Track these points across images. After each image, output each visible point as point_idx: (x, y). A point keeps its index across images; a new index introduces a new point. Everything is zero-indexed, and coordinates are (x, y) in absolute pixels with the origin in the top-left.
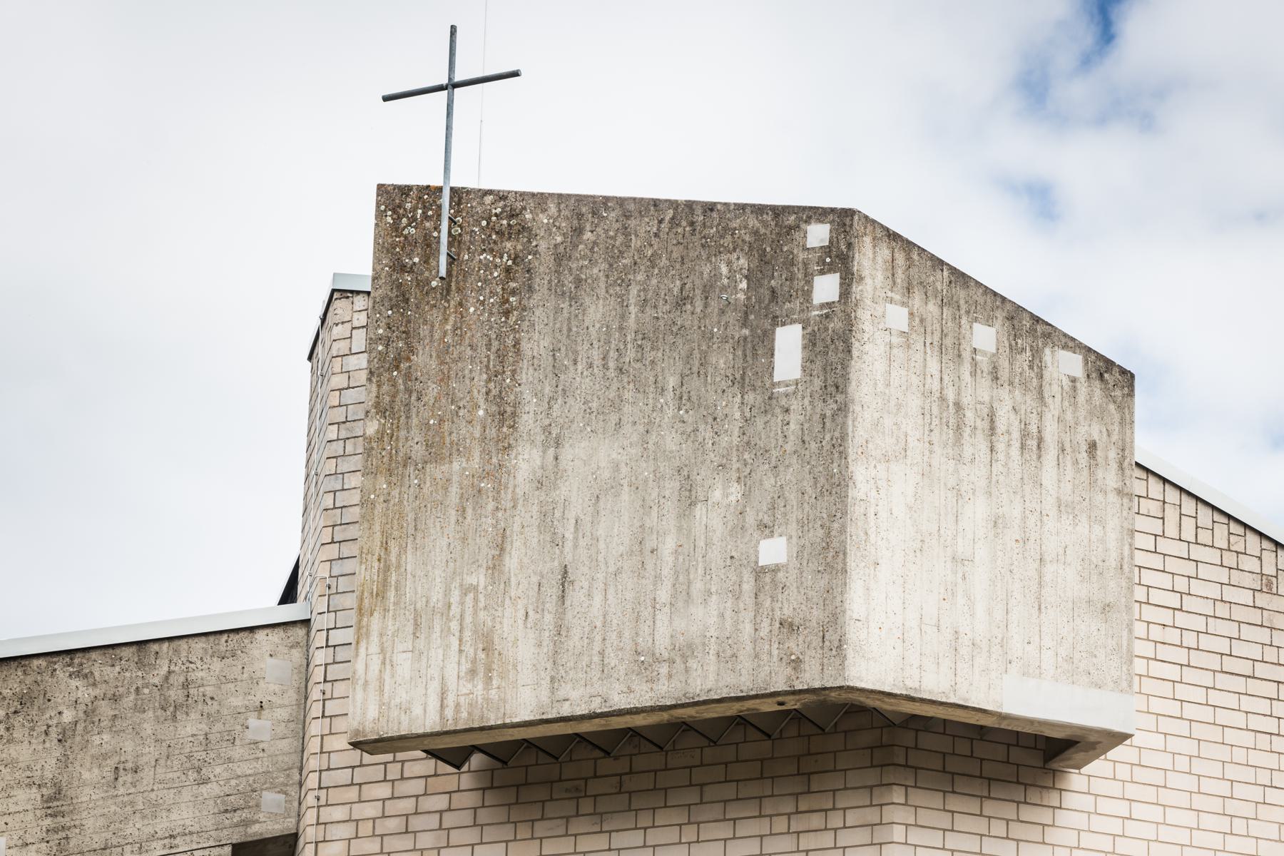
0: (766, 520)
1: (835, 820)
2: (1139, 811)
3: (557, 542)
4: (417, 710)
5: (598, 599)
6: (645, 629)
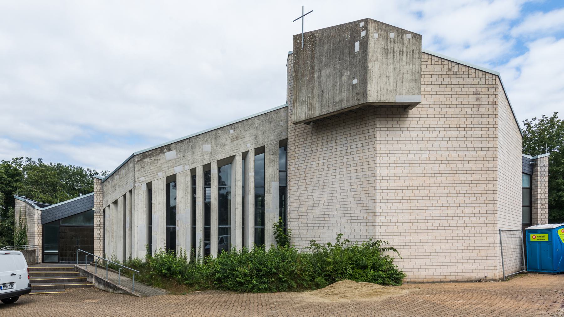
3: (321, 87)
5: (327, 95)
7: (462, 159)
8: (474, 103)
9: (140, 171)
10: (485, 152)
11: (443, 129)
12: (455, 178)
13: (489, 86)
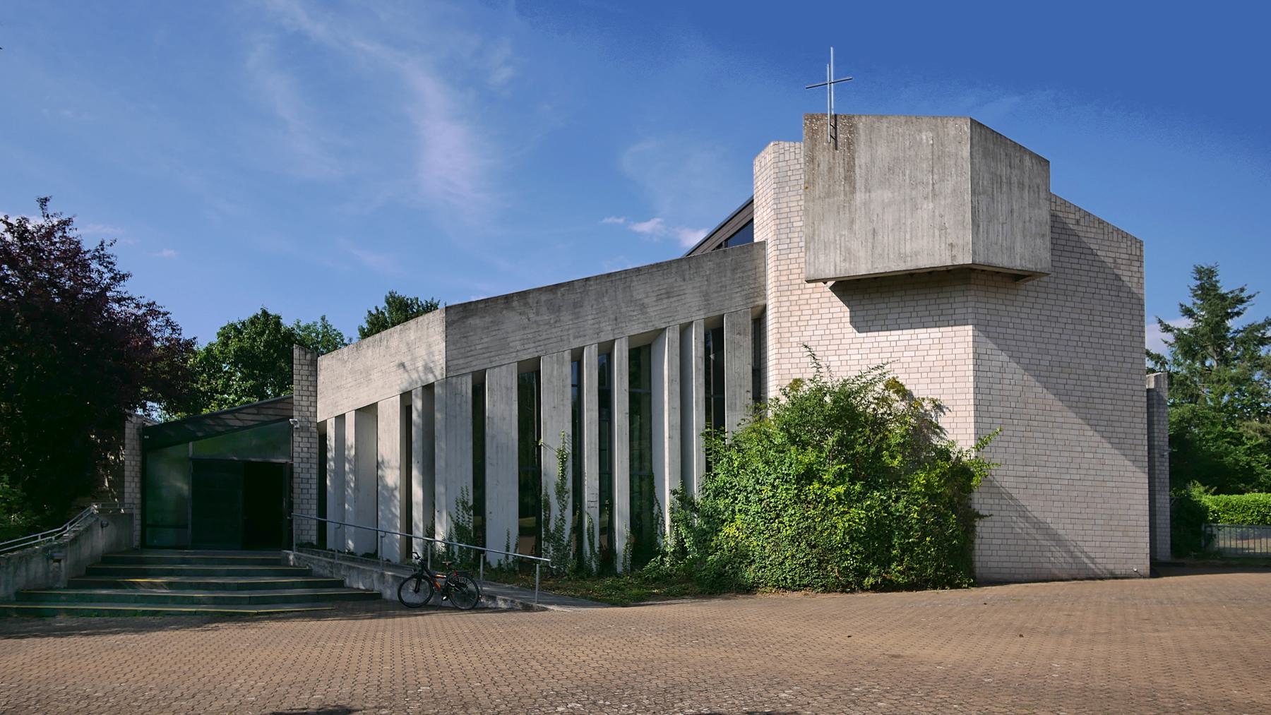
0: (943, 213)
1: (951, 300)
2: (1040, 295)
3: (871, 221)
4: (827, 271)
5: (886, 238)
6: (902, 247)
7: (1097, 373)
8: (1111, 282)
9: (459, 345)
10: (1129, 366)
11: (1070, 321)
12: (1089, 405)
13: (1131, 257)
